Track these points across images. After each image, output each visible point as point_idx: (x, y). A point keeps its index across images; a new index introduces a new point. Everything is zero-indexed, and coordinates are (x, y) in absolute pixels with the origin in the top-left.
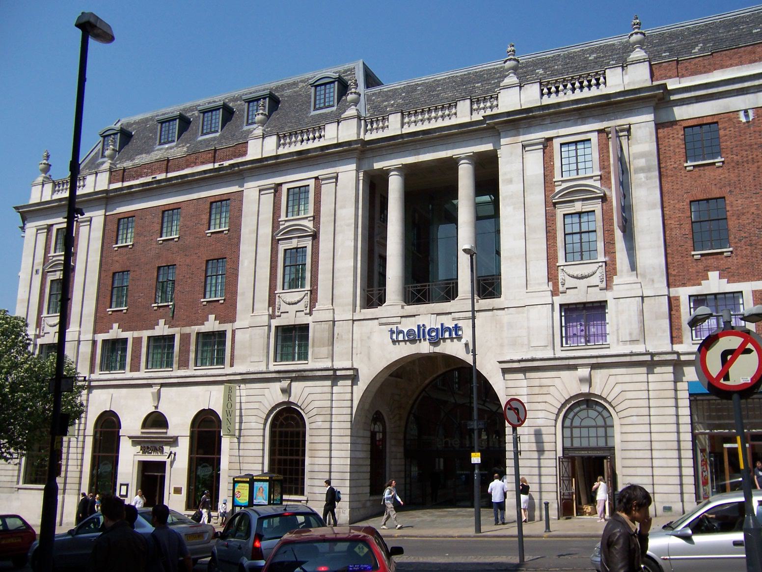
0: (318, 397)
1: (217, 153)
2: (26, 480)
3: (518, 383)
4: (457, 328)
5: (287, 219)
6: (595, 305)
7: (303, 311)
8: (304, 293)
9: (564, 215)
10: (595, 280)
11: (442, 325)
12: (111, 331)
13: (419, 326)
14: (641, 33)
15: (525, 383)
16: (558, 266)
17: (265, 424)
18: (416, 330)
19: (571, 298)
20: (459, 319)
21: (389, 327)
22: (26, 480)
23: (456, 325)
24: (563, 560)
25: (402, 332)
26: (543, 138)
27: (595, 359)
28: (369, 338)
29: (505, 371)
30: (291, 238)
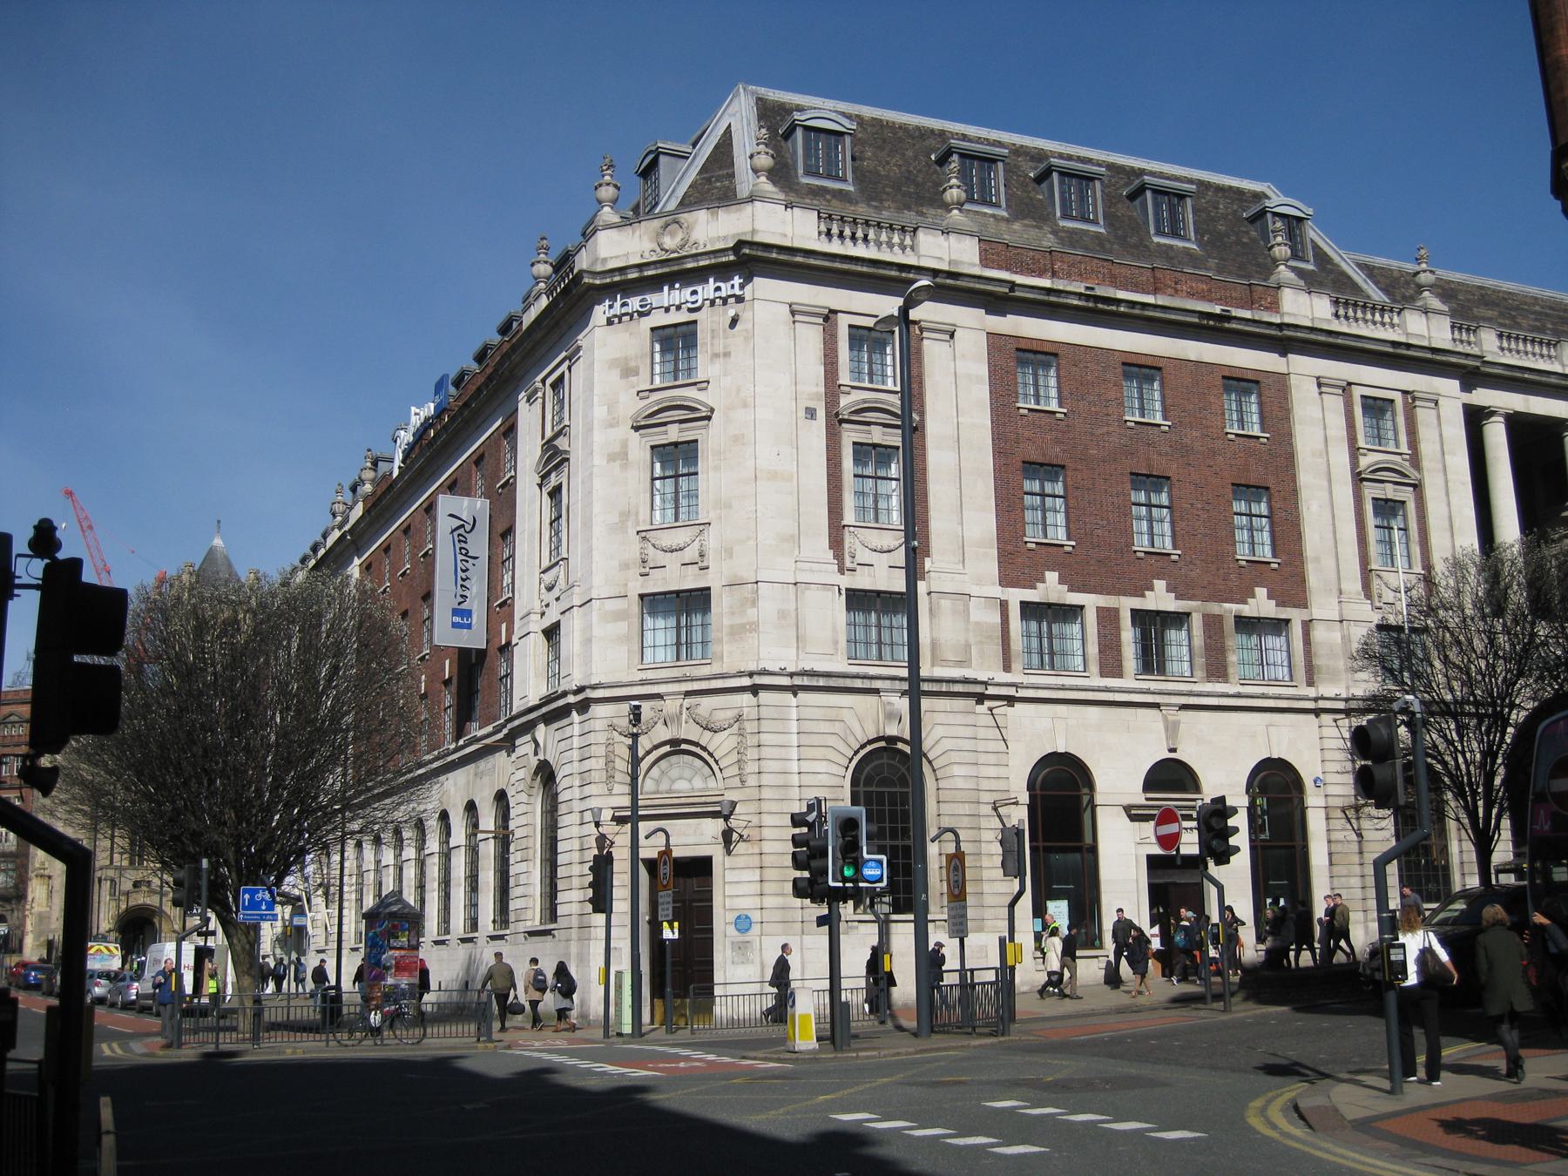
5: (652, 387)
12: (1039, 585)
14: (616, 186)
16: (844, 526)
19: (863, 581)
24: (96, 880)
26: (825, 308)
30: (868, 424)
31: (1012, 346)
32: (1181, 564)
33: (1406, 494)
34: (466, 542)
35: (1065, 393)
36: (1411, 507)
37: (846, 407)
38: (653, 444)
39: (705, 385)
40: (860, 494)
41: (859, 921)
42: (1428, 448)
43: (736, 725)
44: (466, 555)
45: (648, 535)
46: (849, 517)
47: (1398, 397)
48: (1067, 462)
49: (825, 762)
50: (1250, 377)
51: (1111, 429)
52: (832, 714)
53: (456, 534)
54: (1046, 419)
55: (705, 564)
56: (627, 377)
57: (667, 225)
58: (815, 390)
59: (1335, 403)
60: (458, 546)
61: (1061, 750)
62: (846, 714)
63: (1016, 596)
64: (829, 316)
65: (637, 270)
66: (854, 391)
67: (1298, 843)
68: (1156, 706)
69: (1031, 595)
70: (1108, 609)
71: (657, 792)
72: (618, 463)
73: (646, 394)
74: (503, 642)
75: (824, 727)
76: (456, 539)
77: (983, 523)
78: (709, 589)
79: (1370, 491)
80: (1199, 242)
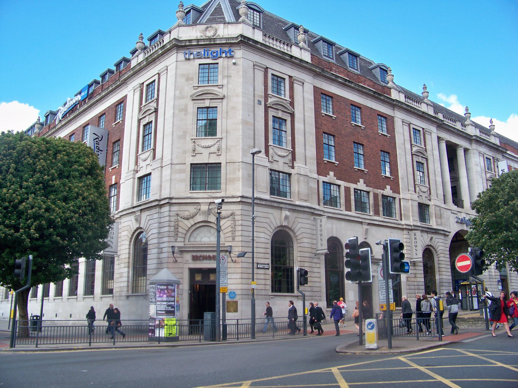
1: (258, 14)
2: (104, 292)
8: (216, 140)
9: (198, 108)
10: (287, 160)
12: (328, 176)
17: (130, 242)
22: (104, 292)
27: (292, 206)
30: (204, 99)
31: (320, 92)
32: (367, 175)
33: (424, 161)
34: (99, 144)
35: (335, 111)
36: (425, 165)
37: (271, 102)
38: (198, 106)
39: (222, 86)
40: (274, 134)
41: (274, 295)
42: (429, 147)
43: (231, 217)
44: (98, 149)
45: (196, 141)
46: (271, 143)
47: (421, 129)
48: (335, 134)
49: (263, 234)
50: (384, 116)
51: (348, 125)
52: (266, 215)
53: (95, 140)
54: (329, 119)
55: (220, 153)
56: (188, 81)
57: (207, 28)
58: (261, 94)
59: (406, 128)
60: (96, 145)
61: (335, 236)
62: (271, 216)
63: (322, 179)
65: (197, 41)
66: (273, 97)
67: (87, 279)
68: (361, 223)
69: (326, 179)
70: (347, 187)
71: (195, 242)
72: (183, 113)
73: (197, 88)
74: (113, 183)
75: (263, 220)
76: (95, 143)
77: (312, 152)
78: (220, 163)
79: (416, 159)
80: (360, 72)
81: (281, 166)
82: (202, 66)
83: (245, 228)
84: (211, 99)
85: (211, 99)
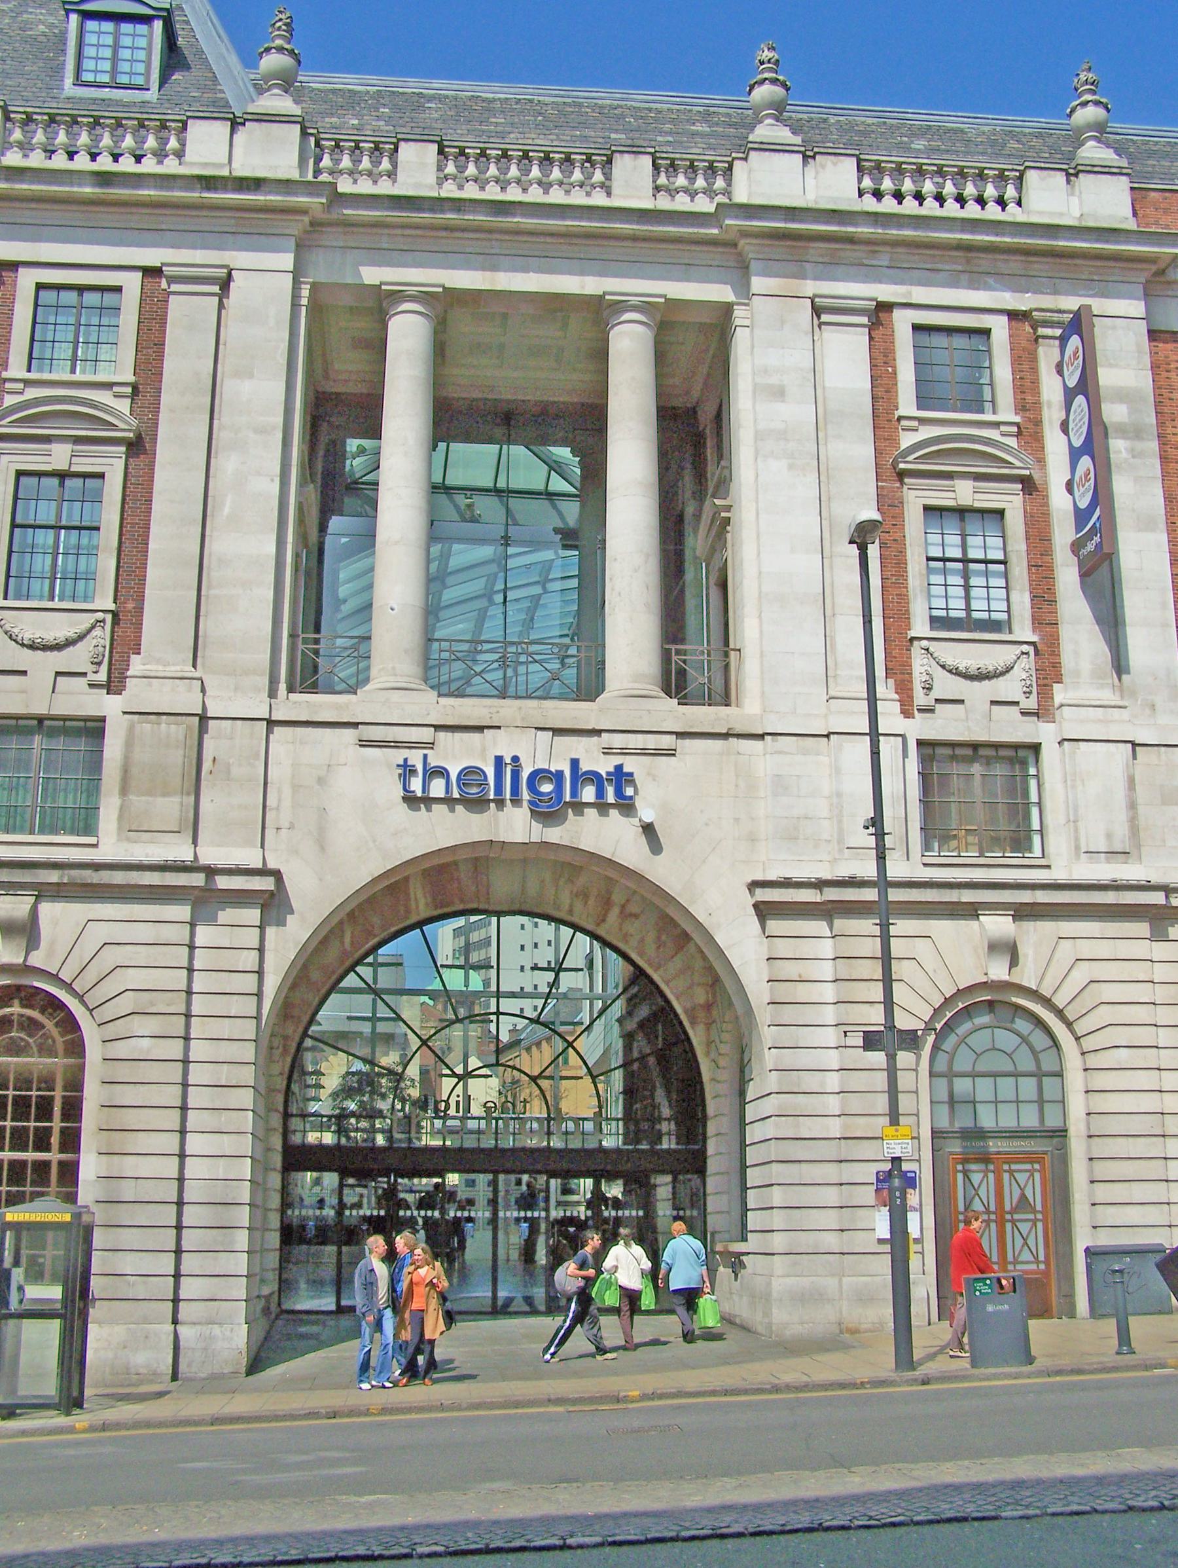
0: (142, 955)
3: (806, 948)
4: (620, 777)
6: (89, 724)
7: (84, 675)
10: (1010, 687)
11: (575, 763)
13: (499, 760)
15: (827, 948)
18: (490, 772)
20: (624, 752)
21: (399, 756)
23: (619, 768)
25: (442, 772)
28: (321, 781)
29: (763, 911)
64: (885, 307)
78: (103, 719)
81: (377, 1335)
82: (48, 297)
83: (855, 1104)
84: (78, 440)
85: (78, 440)
